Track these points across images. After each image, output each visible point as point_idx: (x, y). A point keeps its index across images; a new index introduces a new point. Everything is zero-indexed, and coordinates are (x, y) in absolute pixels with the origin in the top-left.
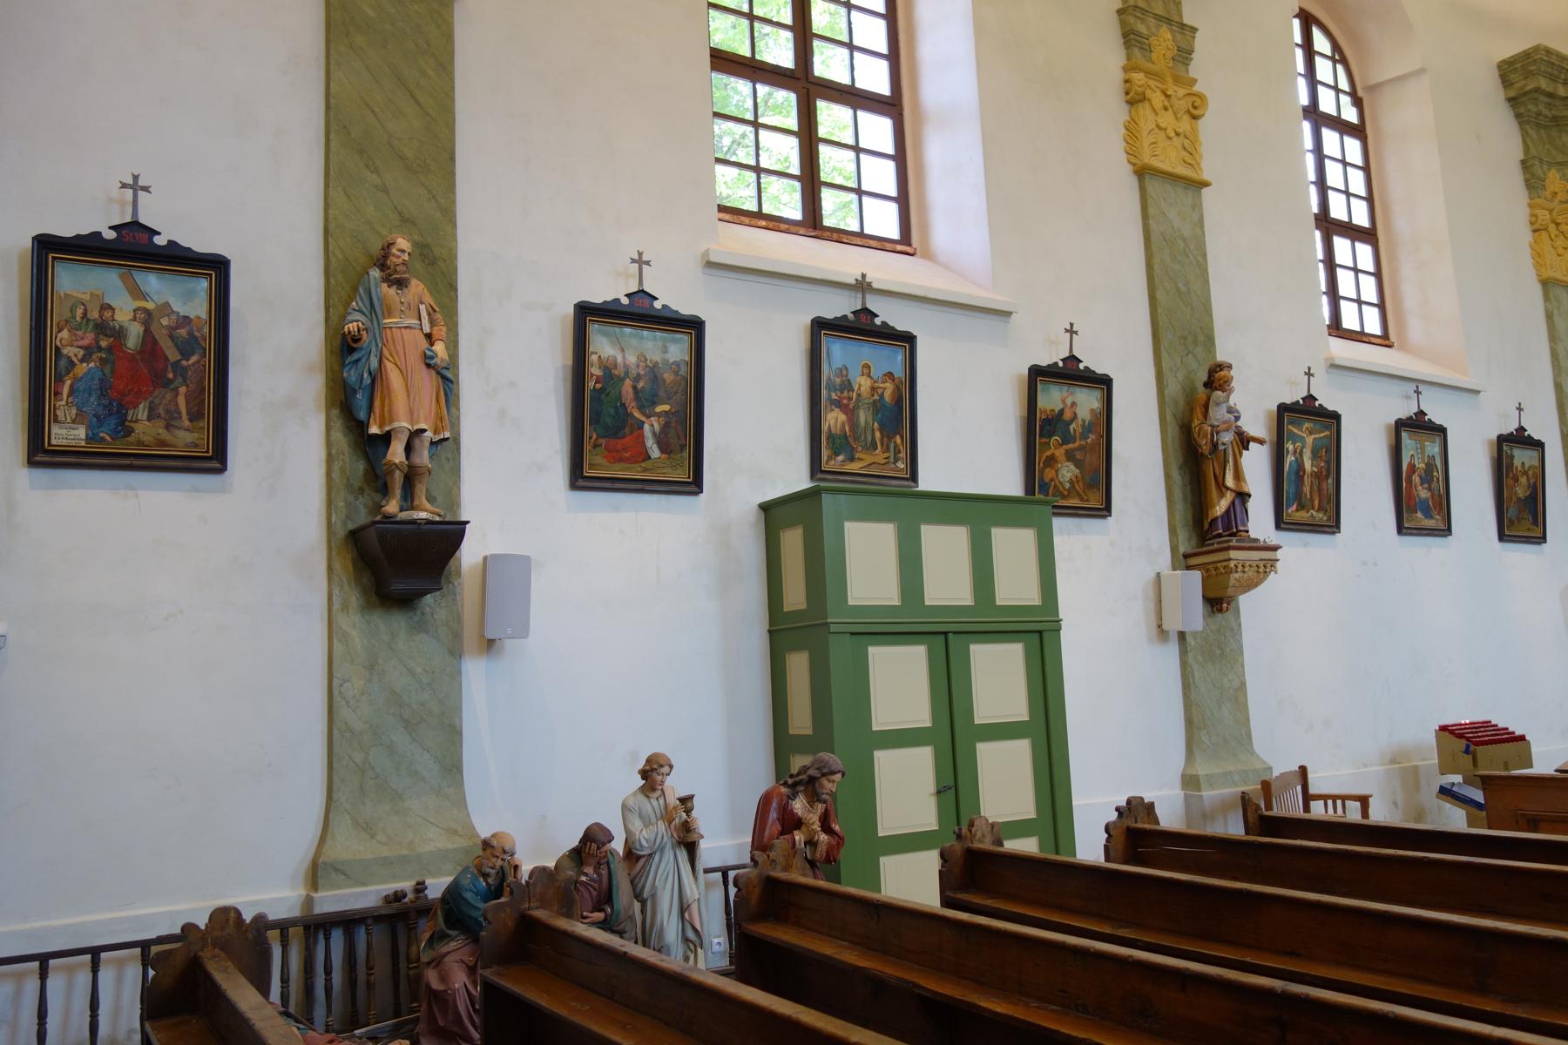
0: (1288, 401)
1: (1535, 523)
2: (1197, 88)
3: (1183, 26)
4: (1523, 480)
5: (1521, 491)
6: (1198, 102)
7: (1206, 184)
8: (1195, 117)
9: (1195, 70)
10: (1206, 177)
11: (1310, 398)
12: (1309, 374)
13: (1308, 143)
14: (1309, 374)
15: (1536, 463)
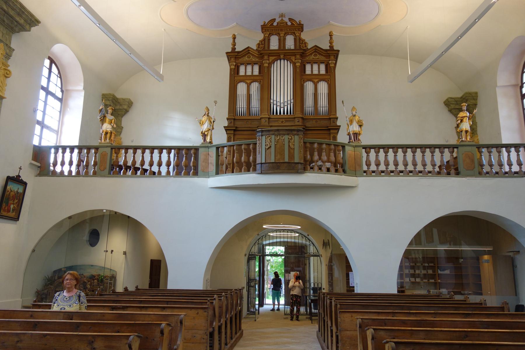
0: (11, 175)
2: (9, 68)
3: (10, 47)
6: (8, 73)
7: (5, 98)
8: (6, 77)
9: (10, 62)
10: (5, 96)
11: (19, 176)
12: (20, 169)
14: (20, 169)
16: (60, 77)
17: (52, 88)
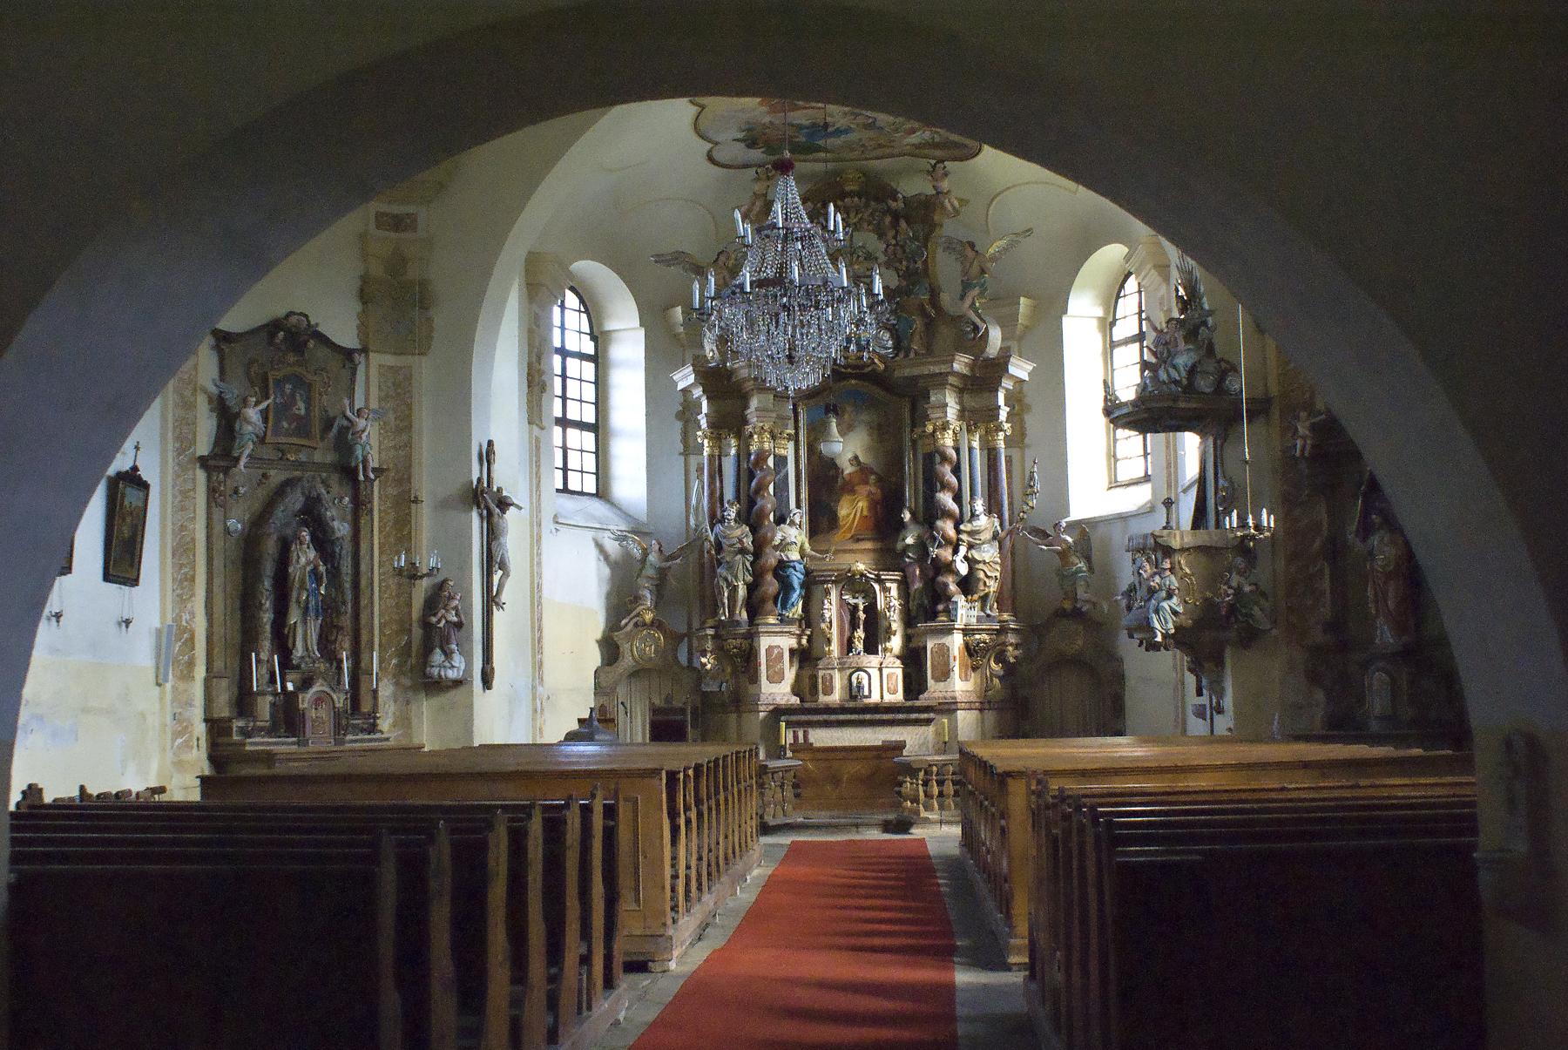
1: (132, 565)
4: (128, 520)
5: (126, 532)
13: (558, 441)
15: (140, 504)
16: (587, 311)
17: (572, 345)
